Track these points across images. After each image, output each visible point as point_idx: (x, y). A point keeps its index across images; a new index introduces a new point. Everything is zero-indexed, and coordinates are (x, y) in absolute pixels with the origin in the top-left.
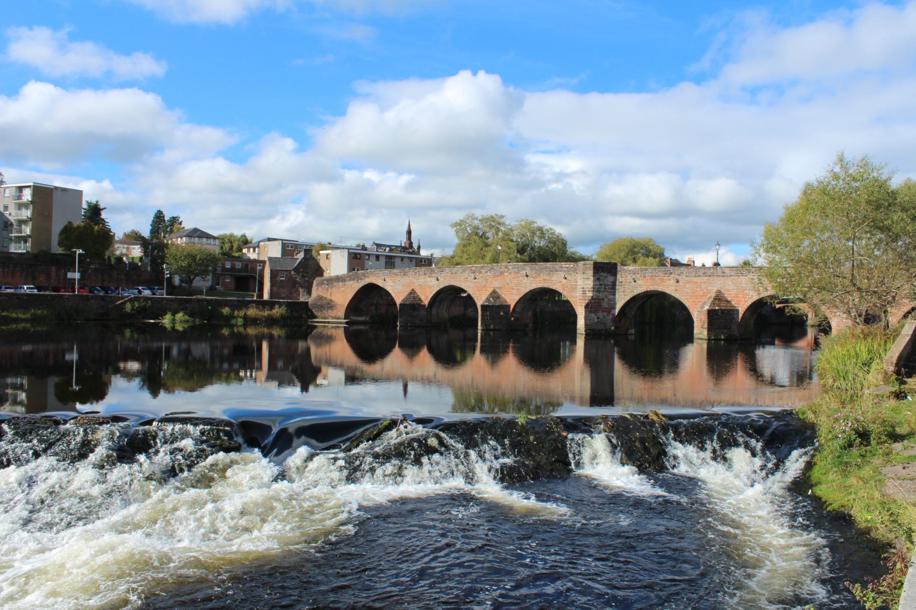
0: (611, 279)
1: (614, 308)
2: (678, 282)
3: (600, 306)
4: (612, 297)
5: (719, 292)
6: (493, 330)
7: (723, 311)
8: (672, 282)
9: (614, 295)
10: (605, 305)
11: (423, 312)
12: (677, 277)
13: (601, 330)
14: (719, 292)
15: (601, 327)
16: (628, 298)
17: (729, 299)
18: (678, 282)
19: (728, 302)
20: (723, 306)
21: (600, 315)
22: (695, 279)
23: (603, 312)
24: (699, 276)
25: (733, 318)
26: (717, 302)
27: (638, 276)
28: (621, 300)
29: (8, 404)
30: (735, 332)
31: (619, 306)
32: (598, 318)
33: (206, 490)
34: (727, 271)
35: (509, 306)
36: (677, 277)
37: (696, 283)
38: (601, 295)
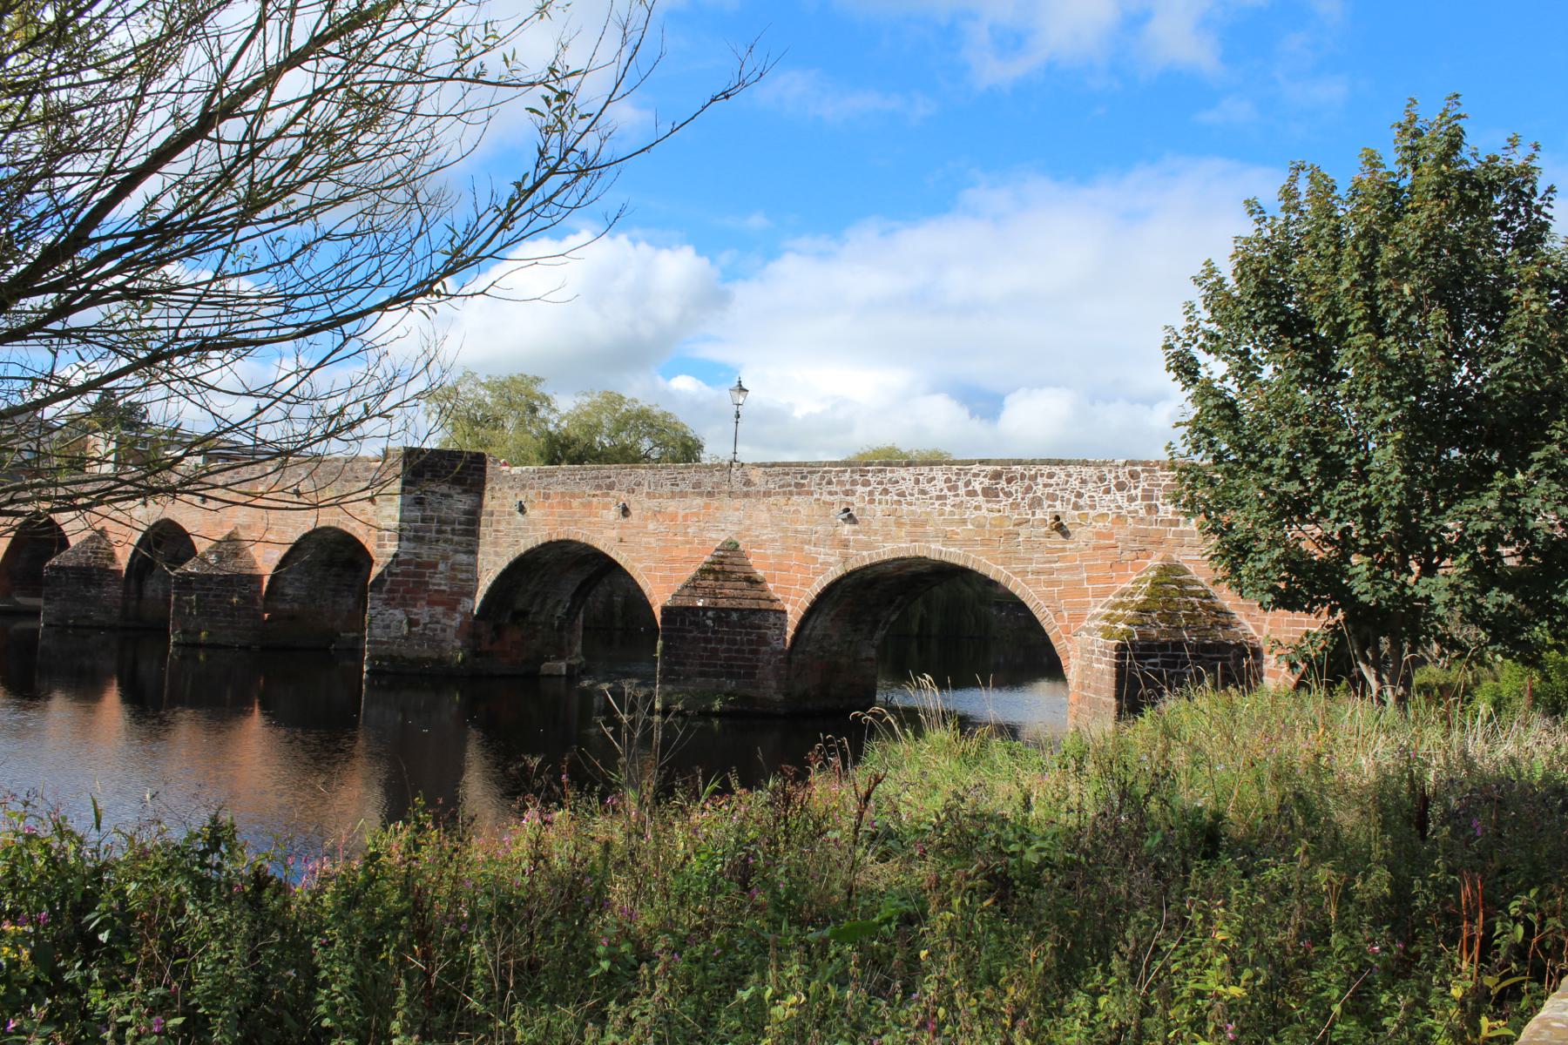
0: (462, 503)
1: (471, 595)
2: (625, 511)
3: (421, 585)
4: (463, 558)
5: (732, 548)
6: (211, 646)
7: (722, 615)
8: (613, 513)
9: (474, 553)
10: (439, 581)
11: (115, 591)
12: (624, 497)
13: (419, 661)
14: (732, 548)
15: (426, 651)
16: (503, 563)
17: (760, 573)
18: (625, 511)
19: (752, 581)
20: (731, 595)
21: (423, 612)
22: (672, 506)
23: (431, 603)
24: (683, 495)
25: (763, 640)
26: (709, 581)
27: (531, 493)
28: (491, 564)
29: (1196, 555)
30: (770, 689)
31: (485, 583)
32: (412, 623)
33: (1266, 656)
34: (756, 476)
35: (258, 579)
36: (624, 497)
37: (673, 517)
38: (425, 552)
